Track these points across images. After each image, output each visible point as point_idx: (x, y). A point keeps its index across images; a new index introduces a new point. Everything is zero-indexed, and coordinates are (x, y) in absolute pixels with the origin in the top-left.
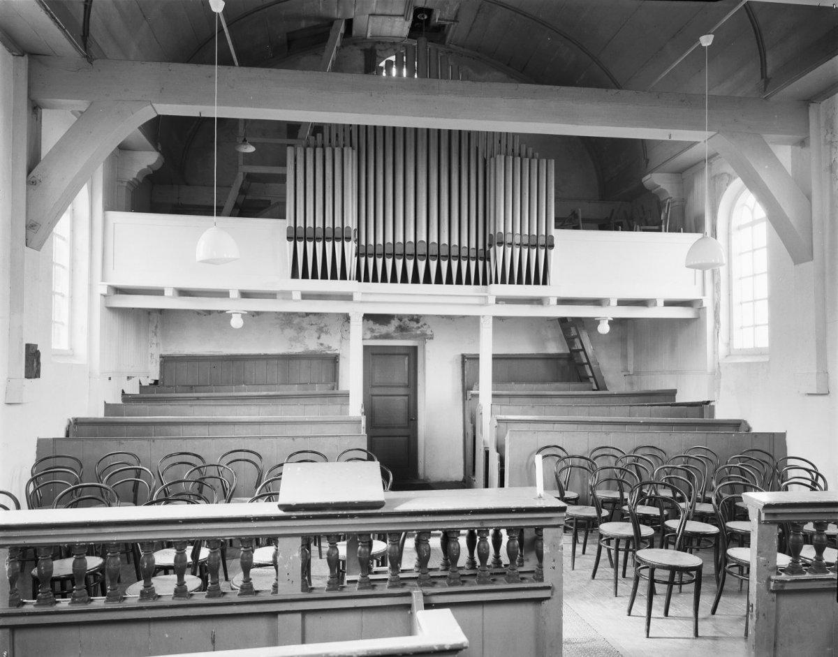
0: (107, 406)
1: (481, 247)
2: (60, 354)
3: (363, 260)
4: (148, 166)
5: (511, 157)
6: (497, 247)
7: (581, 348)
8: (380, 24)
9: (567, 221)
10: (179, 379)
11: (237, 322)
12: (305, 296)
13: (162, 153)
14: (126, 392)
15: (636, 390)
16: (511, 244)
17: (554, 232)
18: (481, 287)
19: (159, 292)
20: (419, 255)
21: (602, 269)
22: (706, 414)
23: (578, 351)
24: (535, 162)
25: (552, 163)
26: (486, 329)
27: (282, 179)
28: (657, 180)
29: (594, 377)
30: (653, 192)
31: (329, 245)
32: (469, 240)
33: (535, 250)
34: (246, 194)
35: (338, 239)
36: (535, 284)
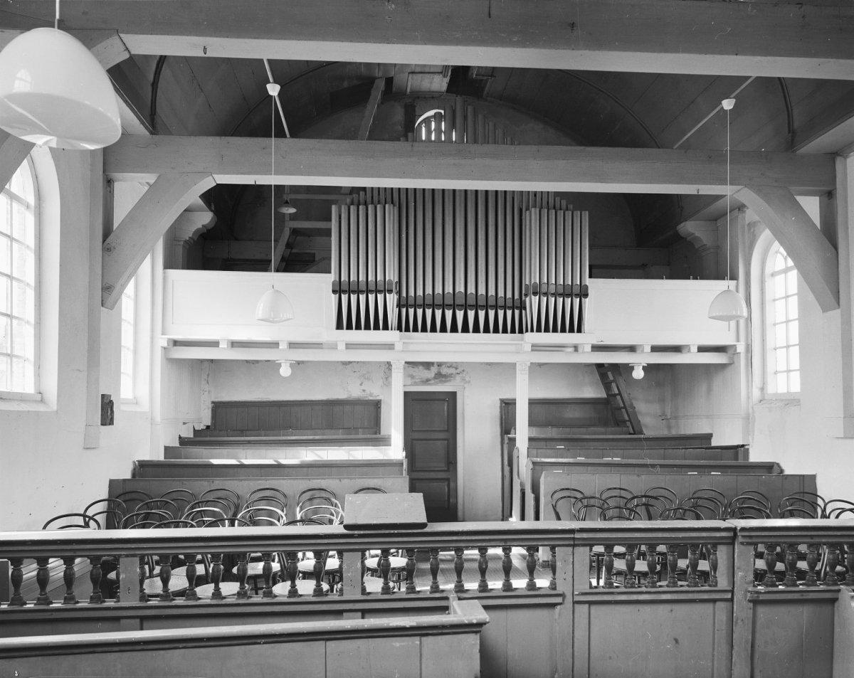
0: (166, 448)
1: (517, 296)
2: (127, 402)
3: (404, 310)
4: (203, 226)
5: (546, 210)
6: (533, 297)
7: (617, 392)
8: (419, 81)
9: (598, 270)
10: (230, 422)
11: (285, 371)
12: (349, 346)
13: (216, 212)
14: (182, 436)
15: (674, 432)
16: (546, 294)
17: (588, 281)
18: (517, 335)
19: (215, 344)
20: (457, 305)
21: (640, 316)
22: (741, 456)
23: (615, 395)
24: (569, 214)
25: (586, 215)
26: (522, 378)
27: (328, 233)
28: (690, 228)
29: (630, 421)
30: (688, 239)
31: (362, 298)
32: (505, 291)
33: (570, 299)
34: (292, 249)
35: (380, 292)
36: (569, 332)
